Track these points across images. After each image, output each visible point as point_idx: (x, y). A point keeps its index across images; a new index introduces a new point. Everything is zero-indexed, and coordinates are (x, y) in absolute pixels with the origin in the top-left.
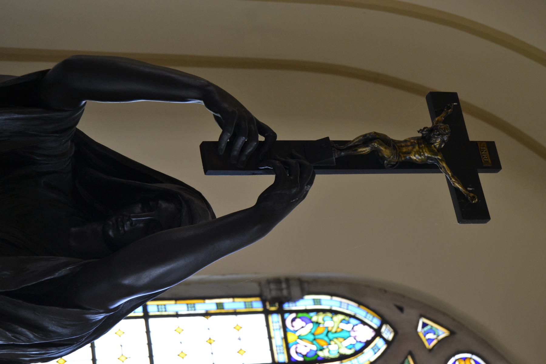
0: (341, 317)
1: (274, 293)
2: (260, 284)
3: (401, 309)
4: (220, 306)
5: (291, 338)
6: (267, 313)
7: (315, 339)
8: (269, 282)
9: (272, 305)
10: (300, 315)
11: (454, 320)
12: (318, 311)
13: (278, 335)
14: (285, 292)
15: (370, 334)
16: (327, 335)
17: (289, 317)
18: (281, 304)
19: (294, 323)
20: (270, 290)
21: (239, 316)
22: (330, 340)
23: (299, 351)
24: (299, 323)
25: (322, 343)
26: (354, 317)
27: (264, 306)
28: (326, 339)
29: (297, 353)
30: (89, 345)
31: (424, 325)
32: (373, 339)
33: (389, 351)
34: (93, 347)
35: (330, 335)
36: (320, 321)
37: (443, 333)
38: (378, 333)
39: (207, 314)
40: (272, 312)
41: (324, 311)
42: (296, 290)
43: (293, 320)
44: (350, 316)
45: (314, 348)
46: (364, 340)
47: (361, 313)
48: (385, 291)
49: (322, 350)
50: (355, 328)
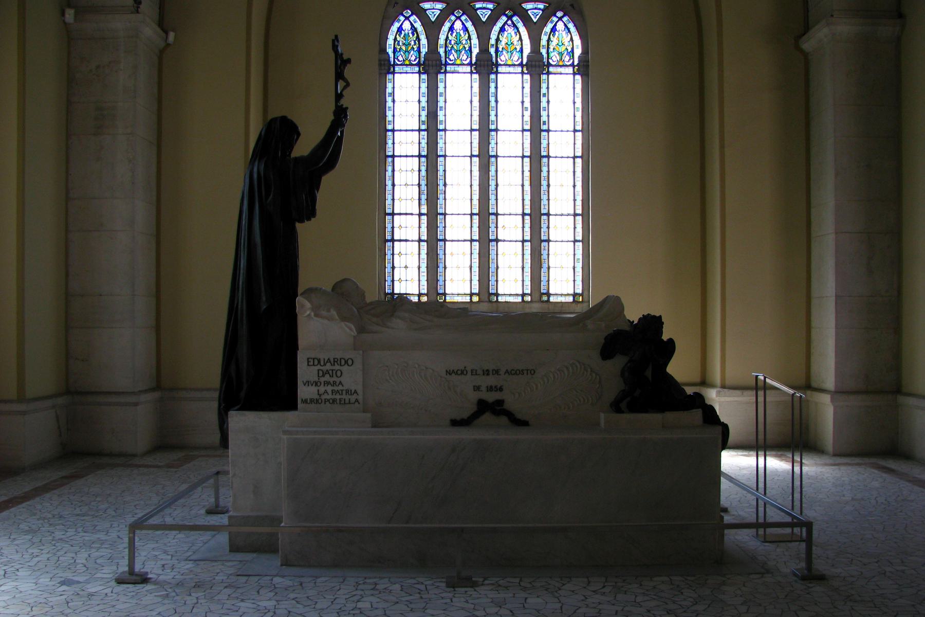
5: (509, 62)
6: (394, 73)
7: (408, 52)
8: (380, 69)
9: (493, 69)
10: (447, 56)
12: (446, 47)
16: (560, 46)
17: (500, 62)
19: (452, 59)
21: (395, 86)
23: (516, 60)
24: (452, 57)
25: (512, 48)
27: (493, 73)
28: (511, 46)
29: (517, 61)
36: (553, 48)
45: (463, 52)
46: (564, 27)
49: (516, 49)
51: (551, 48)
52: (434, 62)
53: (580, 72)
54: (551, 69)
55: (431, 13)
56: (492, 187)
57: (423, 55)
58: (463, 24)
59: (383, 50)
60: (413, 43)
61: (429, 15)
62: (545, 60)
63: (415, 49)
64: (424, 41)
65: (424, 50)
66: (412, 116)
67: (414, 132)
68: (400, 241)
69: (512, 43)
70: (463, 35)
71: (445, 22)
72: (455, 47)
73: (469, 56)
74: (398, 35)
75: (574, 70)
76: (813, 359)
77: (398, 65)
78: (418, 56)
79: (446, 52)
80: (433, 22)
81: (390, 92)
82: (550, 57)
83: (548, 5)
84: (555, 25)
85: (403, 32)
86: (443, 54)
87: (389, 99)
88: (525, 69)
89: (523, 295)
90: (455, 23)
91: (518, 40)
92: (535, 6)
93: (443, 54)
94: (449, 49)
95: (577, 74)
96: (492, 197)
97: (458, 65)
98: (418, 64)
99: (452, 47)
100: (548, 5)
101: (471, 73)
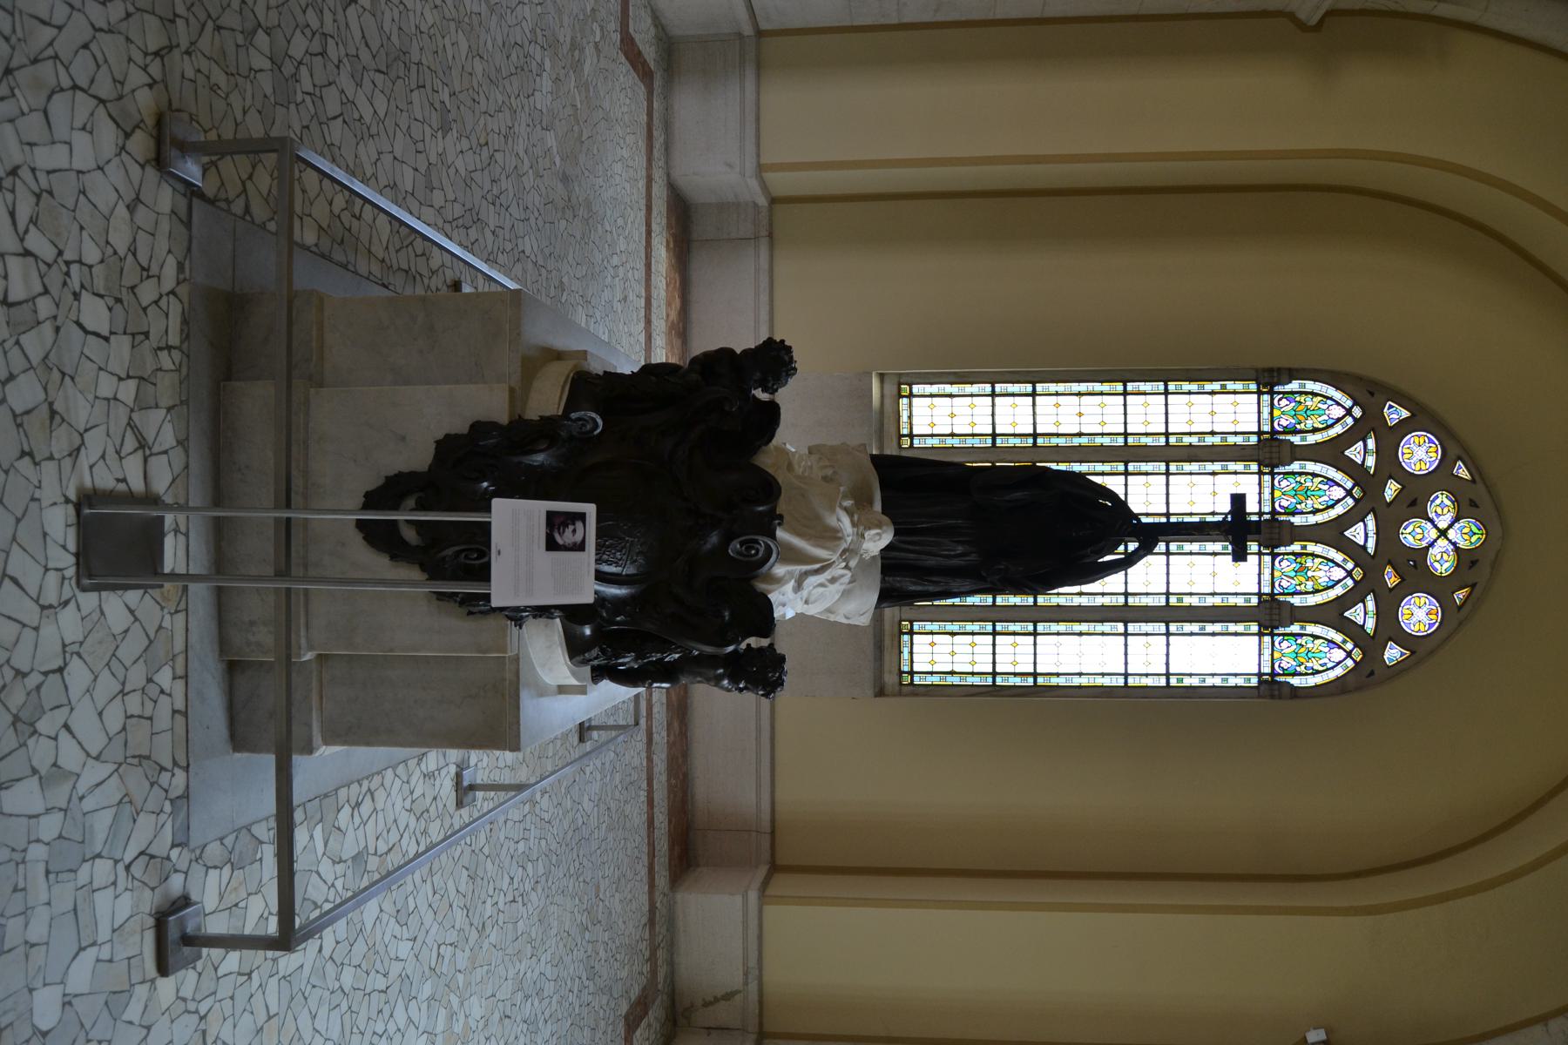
0: (1320, 398)
1: (1266, 380)
2: (1257, 370)
3: (1372, 394)
4: (1223, 387)
5: (1276, 413)
6: (1260, 634)
7: (1296, 495)
8: (1264, 370)
9: (1266, 466)
11: (1417, 404)
12: (1301, 393)
13: (1267, 491)
14: (1275, 380)
15: (1342, 412)
17: (1277, 639)
18: (1272, 388)
20: (1264, 377)
22: (1308, 497)
24: (1284, 402)
26: (1331, 399)
27: (1259, 388)
30: (1124, 572)
31: (1391, 407)
32: (1345, 578)
33: (1355, 428)
34: (1126, 574)
35: (1309, 413)
36: (1302, 401)
37: (1405, 414)
38: (1349, 412)
39: (1213, 393)
40: (1266, 473)
41: (1306, 393)
42: (1285, 377)
43: (1280, 400)
44: (1328, 398)
45: (1293, 421)
46: (1336, 579)
47: (1338, 395)
48: (1361, 379)
50: (1330, 408)
51: (1302, 399)
52: (1277, 536)
53: (1261, 444)
54: (1267, 559)
55: (1358, 450)
56: (1077, 627)
57: (1289, 599)
58: (1340, 581)
59: (1292, 375)
60: (1309, 665)
61: (1354, 527)
62: (1281, 630)
63: (1298, 506)
64: (1312, 600)
65: (1296, 601)
66: (1191, 583)
67: (1165, 505)
68: (993, 405)
69: (1308, 497)
70: (1320, 419)
71: (1344, 634)
72: (1301, 408)
73: (1286, 591)
74: (1321, 398)
75: (1267, 634)
76: (813, 23)
77: (1273, 479)
78: (1287, 511)
79: (1293, 393)
80: (1343, 452)
81: (1228, 387)
82: (1286, 476)
83: (1372, 472)
84: (1339, 485)
85: (1327, 486)
86: (1288, 388)
87: (1216, 386)
88: (1267, 517)
89: (911, 436)
90: (1341, 650)
91: (1315, 668)
92: (1371, 614)
93: (1288, 388)
94: (1298, 399)
95: (1259, 599)
96: (1062, 627)
97: (1272, 655)
98: (1273, 432)
99: (1303, 646)
100: (1372, 472)
101: (1260, 594)
